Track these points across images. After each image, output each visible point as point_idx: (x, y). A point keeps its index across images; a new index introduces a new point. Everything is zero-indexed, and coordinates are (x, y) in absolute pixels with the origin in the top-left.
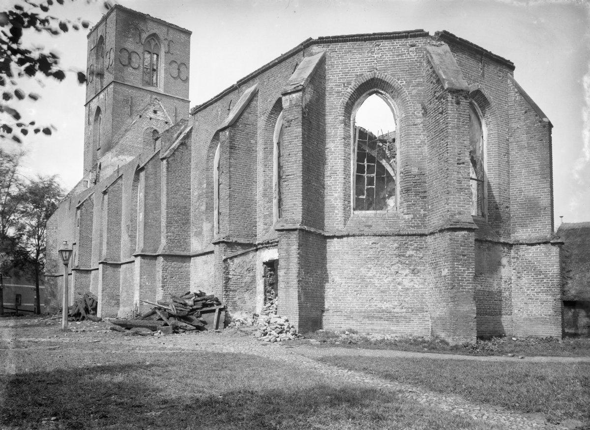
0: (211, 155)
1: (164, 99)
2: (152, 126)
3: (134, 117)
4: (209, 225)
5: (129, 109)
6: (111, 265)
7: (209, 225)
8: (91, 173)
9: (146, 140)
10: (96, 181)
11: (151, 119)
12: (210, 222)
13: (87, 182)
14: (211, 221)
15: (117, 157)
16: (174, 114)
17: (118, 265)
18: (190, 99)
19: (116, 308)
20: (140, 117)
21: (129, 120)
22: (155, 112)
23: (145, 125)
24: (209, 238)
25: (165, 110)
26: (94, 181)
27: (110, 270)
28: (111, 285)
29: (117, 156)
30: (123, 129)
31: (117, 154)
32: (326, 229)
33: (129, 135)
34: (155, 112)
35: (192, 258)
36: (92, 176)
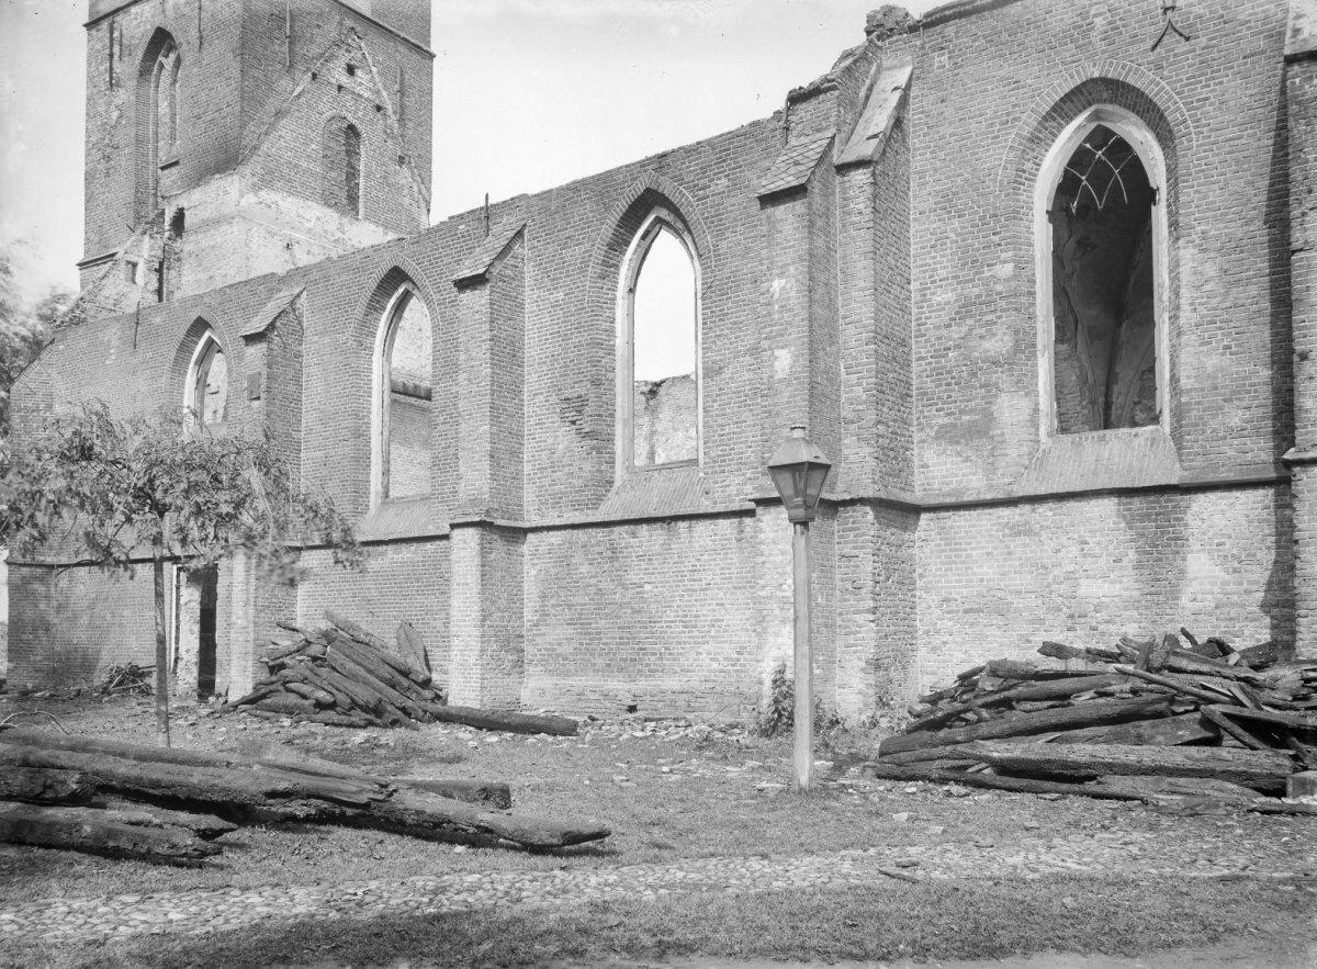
0: (1028, 166)
1: (373, 35)
2: (344, 113)
3: (298, 74)
4: (1025, 404)
5: (286, 48)
6: (503, 530)
7: (1025, 404)
8: (147, 237)
9: (329, 153)
10: (161, 264)
11: (340, 88)
12: (1026, 395)
13: (135, 265)
14: (1031, 392)
15: (256, 193)
16: (397, 87)
17: (516, 534)
18: (433, 49)
19: (514, 678)
20: (314, 76)
21: (285, 83)
22: (351, 70)
23: (326, 107)
24: (1025, 449)
25: (374, 70)
26: (157, 266)
27: (499, 545)
28: (503, 603)
29: (255, 188)
30: (270, 108)
31: (254, 185)
32: (918, 479)
33: (287, 128)
34: (351, 70)
35: (924, 517)
36: (152, 248)
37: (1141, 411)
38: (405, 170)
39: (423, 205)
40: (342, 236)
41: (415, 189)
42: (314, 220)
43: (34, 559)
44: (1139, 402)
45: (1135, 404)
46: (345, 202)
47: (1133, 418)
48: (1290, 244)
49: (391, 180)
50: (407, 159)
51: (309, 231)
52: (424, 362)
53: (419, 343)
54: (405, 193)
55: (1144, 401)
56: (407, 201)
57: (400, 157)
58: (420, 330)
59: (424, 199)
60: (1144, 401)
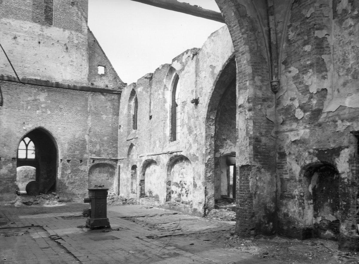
9: (35, 3)
37: (292, 31)
38: (75, 8)
39: (83, 19)
40: (42, 33)
41: (80, 13)
42: (28, 28)
43: (315, 83)
44: (290, 26)
45: (289, 27)
46: (43, 20)
47: (288, 37)
48: (314, 206)
49: (68, 11)
50: (76, 3)
51: (26, 32)
52: (83, 77)
53: (81, 70)
54: (74, 15)
55: (293, 24)
56: (75, 18)
57: (72, 2)
58: (81, 65)
59: (84, 17)
60: (293, 24)
